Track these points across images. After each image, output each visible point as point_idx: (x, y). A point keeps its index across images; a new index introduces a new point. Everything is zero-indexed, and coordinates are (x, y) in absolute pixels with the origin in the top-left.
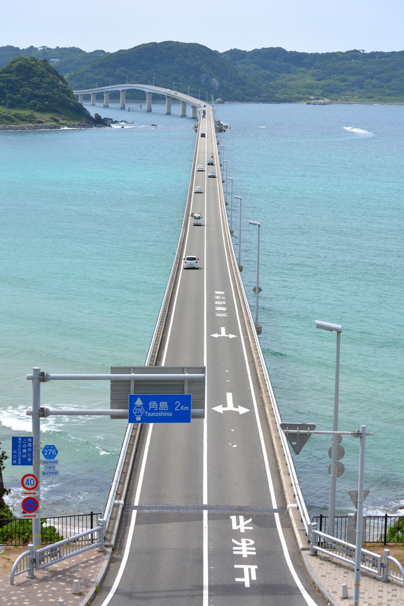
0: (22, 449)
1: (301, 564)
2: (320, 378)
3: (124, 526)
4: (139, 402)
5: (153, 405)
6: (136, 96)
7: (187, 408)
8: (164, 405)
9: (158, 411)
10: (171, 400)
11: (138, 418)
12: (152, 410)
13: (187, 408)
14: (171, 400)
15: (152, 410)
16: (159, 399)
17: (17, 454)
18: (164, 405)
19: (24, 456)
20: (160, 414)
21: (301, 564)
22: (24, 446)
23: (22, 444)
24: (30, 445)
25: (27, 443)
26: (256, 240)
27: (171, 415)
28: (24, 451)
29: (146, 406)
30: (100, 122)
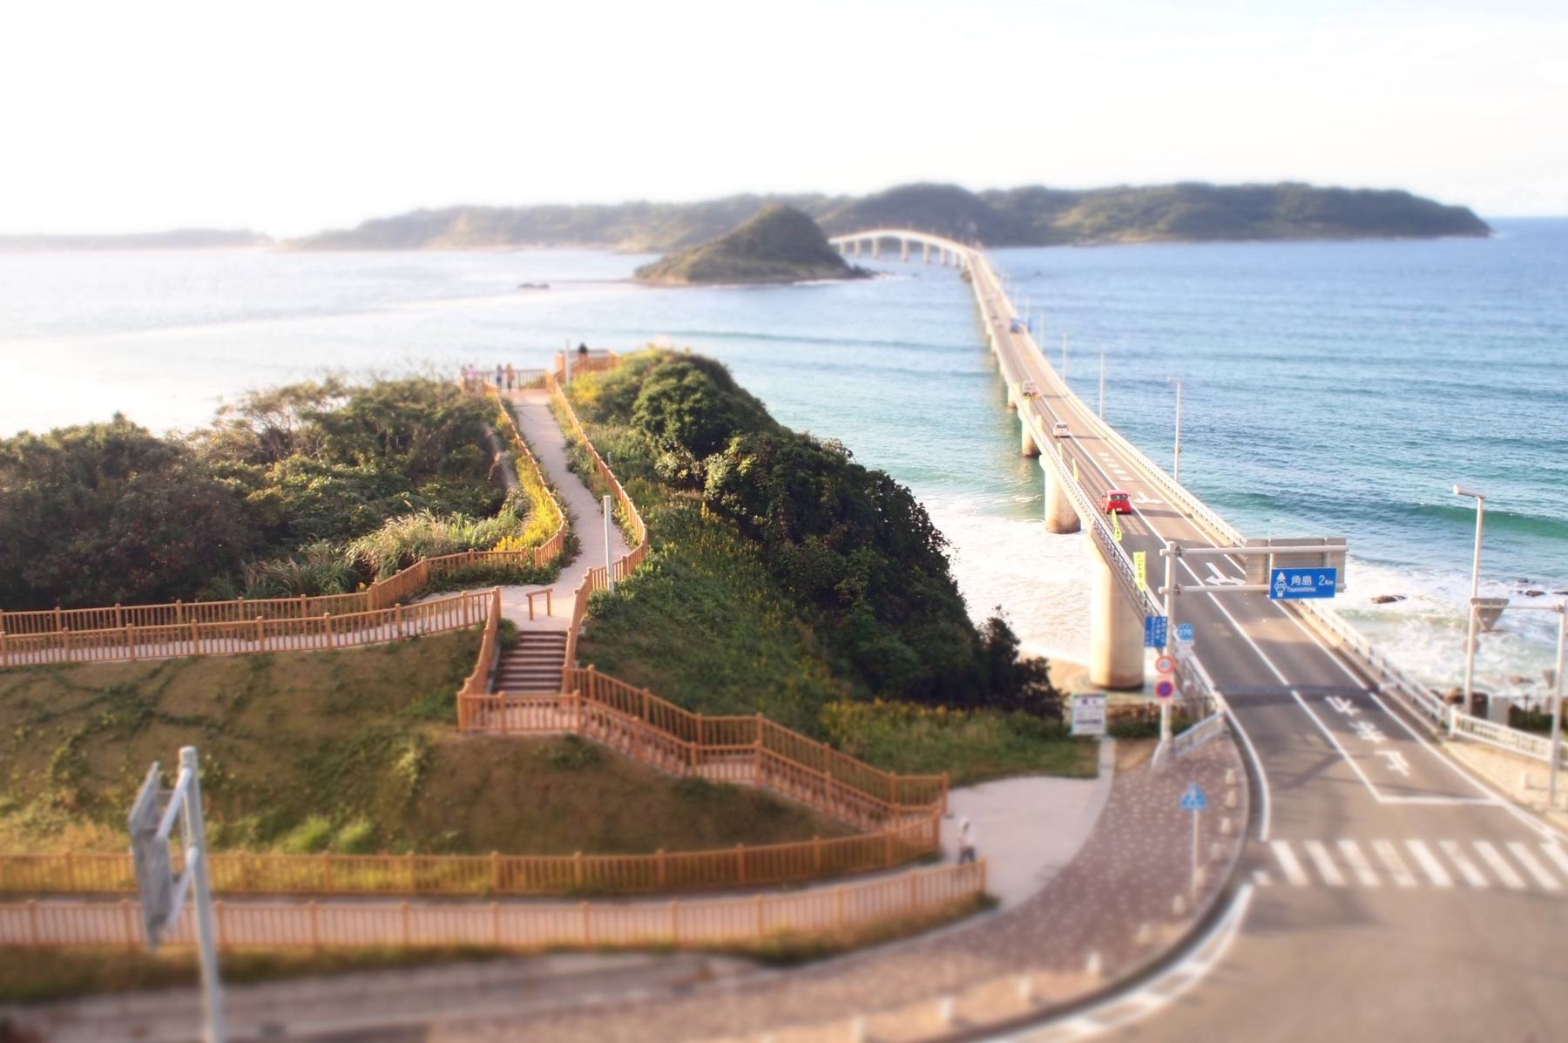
0: (1156, 629)
1: (1227, 634)
2: (537, 867)
3: (416, 399)
4: (1281, 577)
5: (1296, 579)
6: (890, 245)
7: (1331, 583)
8: (1307, 580)
9: (1302, 586)
10: (1315, 574)
11: (1280, 594)
12: (1295, 586)
13: (1331, 583)
14: (1315, 574)
15: (1295, 586)
16: (1302, 573)
17: (1150, 635)
18: (1307, 580)
19: (1158, 637)
20: (1303, 590)
21: (1227, 634)
22: (1158, 626)
23: (1156, 624)
24: (1164, 625)
25: (1161, 622)
26: (1147, 948)
27: (1314, 590)
28: (1158, 631)
29: (1288, 581)
30: (859, 273)
